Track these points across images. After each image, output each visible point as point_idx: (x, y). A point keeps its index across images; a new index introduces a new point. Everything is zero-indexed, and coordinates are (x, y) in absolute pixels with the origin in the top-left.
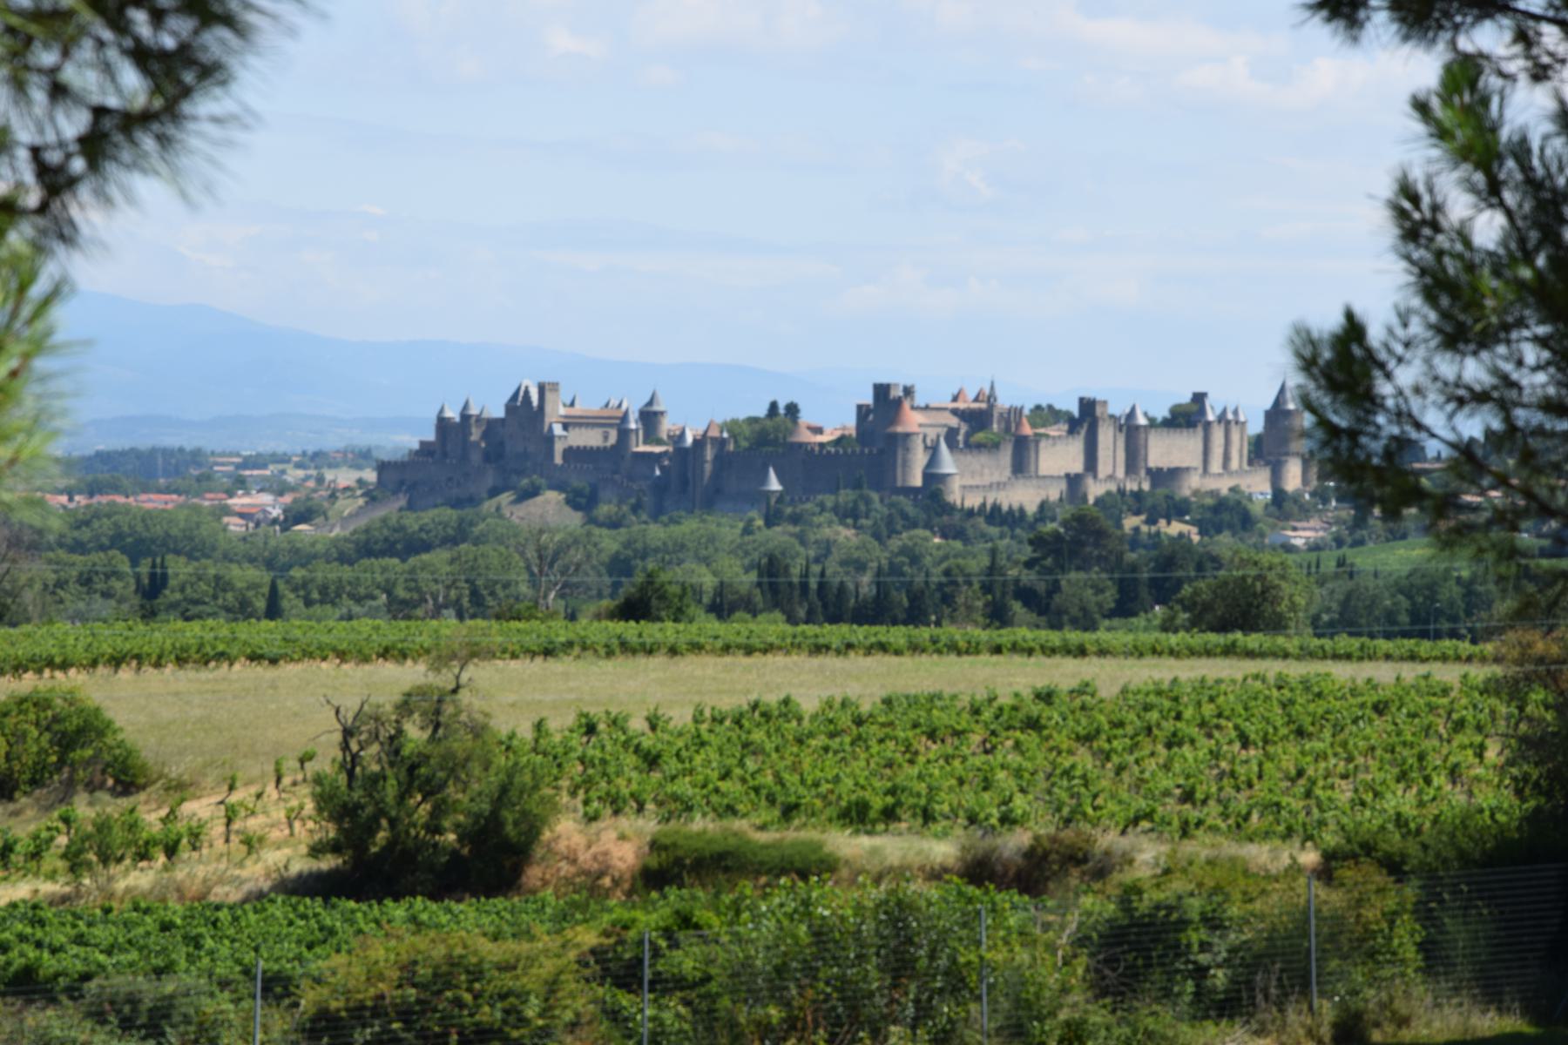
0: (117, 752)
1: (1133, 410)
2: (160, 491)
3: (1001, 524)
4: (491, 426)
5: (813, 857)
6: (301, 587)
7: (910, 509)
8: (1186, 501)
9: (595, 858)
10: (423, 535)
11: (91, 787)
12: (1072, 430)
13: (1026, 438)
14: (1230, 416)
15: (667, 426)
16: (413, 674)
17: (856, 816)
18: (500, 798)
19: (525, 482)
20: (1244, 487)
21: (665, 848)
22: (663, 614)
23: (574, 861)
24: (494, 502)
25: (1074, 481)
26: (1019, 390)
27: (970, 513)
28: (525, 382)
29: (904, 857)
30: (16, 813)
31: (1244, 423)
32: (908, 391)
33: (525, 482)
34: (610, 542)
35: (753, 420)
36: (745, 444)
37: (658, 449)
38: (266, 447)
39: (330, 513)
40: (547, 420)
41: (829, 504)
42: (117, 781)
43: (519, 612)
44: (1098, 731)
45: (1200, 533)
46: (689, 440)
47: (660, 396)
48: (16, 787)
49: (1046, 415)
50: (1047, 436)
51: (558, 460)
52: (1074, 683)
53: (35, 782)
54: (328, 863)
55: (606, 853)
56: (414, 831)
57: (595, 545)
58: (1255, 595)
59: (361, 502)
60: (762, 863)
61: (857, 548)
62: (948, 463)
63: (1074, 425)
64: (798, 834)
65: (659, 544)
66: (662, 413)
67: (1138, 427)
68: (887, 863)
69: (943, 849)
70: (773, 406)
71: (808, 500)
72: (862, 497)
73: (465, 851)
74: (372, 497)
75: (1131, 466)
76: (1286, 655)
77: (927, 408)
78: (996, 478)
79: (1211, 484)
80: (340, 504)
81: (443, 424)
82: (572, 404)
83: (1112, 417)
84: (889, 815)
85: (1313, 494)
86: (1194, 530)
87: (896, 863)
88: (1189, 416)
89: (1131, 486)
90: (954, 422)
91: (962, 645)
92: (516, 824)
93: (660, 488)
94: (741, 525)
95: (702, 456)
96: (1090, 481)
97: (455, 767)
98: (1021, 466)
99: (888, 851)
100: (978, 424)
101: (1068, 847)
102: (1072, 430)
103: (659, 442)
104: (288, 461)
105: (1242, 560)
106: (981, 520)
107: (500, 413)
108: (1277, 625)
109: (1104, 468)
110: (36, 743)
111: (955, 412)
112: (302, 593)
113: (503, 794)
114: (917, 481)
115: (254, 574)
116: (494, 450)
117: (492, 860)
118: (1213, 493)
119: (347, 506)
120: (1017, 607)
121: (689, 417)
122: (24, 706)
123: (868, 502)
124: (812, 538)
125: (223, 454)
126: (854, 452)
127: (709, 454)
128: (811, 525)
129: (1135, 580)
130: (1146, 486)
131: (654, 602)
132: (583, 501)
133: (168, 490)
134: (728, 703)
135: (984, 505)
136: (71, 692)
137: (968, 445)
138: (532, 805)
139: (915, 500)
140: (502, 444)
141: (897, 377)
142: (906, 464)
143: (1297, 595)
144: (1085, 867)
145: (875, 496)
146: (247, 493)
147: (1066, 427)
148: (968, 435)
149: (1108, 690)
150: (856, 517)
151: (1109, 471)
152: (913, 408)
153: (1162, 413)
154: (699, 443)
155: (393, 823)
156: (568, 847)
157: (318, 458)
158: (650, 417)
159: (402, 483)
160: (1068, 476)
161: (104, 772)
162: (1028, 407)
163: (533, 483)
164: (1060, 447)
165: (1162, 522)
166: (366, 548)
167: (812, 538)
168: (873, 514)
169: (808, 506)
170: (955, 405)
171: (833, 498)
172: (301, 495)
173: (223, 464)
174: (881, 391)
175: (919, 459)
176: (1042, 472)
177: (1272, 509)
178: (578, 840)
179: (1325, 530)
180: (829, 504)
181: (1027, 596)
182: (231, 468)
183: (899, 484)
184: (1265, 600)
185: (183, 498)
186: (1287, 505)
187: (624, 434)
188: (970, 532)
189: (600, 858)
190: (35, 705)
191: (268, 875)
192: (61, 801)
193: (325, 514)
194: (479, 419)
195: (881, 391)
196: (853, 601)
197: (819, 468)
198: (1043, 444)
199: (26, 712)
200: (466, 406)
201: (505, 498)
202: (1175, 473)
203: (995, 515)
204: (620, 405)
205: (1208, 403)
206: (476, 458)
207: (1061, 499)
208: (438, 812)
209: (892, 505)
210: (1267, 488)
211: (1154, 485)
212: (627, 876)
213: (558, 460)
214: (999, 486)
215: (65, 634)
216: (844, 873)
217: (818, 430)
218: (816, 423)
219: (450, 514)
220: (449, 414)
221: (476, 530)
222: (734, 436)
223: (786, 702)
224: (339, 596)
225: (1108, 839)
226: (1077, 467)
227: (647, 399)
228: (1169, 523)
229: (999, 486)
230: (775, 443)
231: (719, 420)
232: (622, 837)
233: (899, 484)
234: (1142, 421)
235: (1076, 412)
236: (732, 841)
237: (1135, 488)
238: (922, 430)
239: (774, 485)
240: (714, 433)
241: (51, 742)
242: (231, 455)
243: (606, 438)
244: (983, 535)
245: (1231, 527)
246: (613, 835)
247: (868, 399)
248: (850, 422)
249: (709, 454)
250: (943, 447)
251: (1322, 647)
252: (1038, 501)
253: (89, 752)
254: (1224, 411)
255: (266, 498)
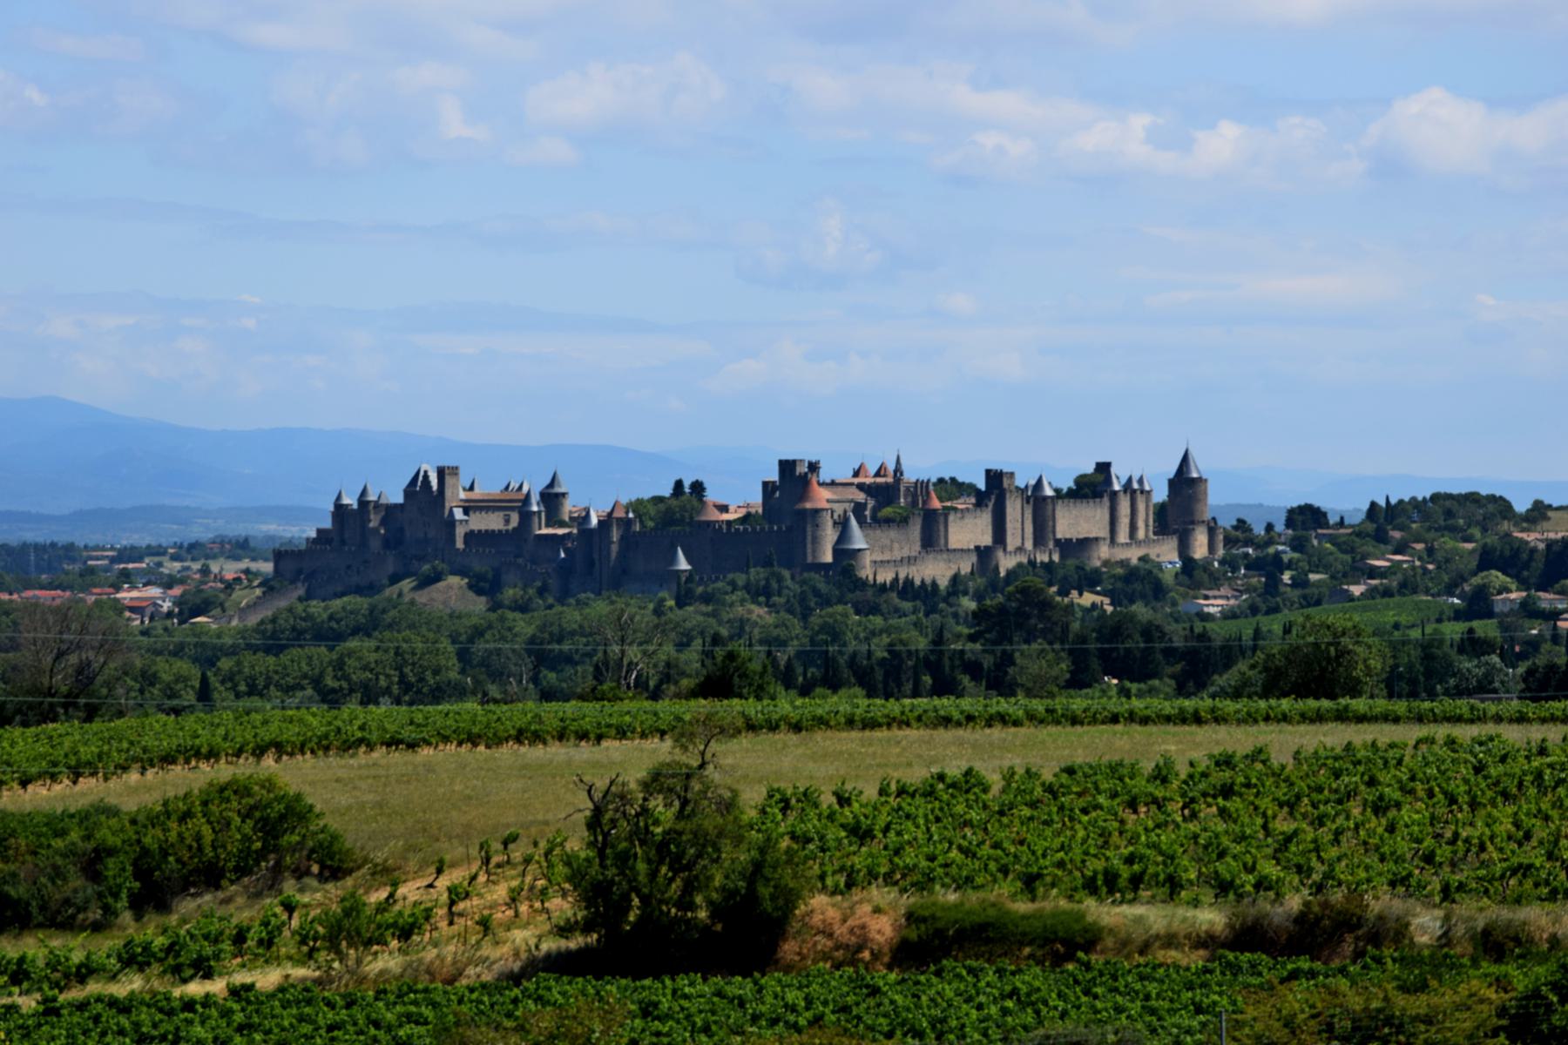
0: (321, 836)
1: (1040, 481)
2: (42, 587)
3: (914, 599)
4: (390, 512)
5: (1077, 927)
6: (229, 679)
7: (823, 587)
8: (1096, 571)
9: (851, 931)
10: (334, 625)
11: (300, 873)
12: (980, 504)
13: (935, 511)
14: (1136, 486)
15: (569, 507)
16: (662, 750)
17: (1107, 885)
18: (754, 873)
19: (426, 567)
20: (1153, 557)
21: (924, 920)
22: (745, 691)
23: (830, 935)
24: (395, 589)
25: (984, 554)
26: (921, 467)
27: (883, 588)
28: (424, 467)
29: (1170, 924)
30: (227, 901)
31: (1149, 492)
32: (814, 467)
33: (426, 567)
34: (524, 626)
35: (658, 500)
36: (651, 524)
37: (561, 531)
38: (142, 540)
39: (227, 605)
40: (447, 505)
41: (740, 583)
42: (323, 867)
43: (603, 693)
44: (1298, 797)
45: (1112, 604)
46: (594, 521)
47: (561, 477)
48: (222, 876)
49: (952, 487)
50: (955, 509)
51: (460, 544)
52: (1248, 750)
53: (242, 871)
54: (575, 943)
55: (863, 927)
56: (667, 907)
57: (510, 629)
58: (1329, 659)
59: (258, 592)
60: (1024, 934)
61: (776, 627)
62: (859, 540)
63: (981, 499)
64: (1054, 902)
65: (575, 626)
66: (564, 495)
67: (1045, 498)
68: (1153, 932)
69: (1211, 917)
70: (679, 485)
71: (717, 579)
72: (773, 574)
73: (719, 927)
74: (269, 587)
75: (1039, 540)
76: (1397, 720)
77: (833, 483)
78: (906, 553)
79: (1121, 554)
80: (237, 594)
81: (340, 510)
82: (471, 488)
83: (1018, 488)
84: (1136, 881)
85: (1222, 562)
86: (1107, 600)
87: (1162, 932)
88: (1094, 486)
89: (1042, 557)
90: (861, 497)
91: (956, 715)
92: (773, 898)
93: (566, 569)
94: (651, 606)
95: (609, 537)
96: (1000, 554)
97: (707, 844)
98: (931, 540)
99: (1152, 919)
100: (886, 499)
101: (1339, 913)
102: (980, 504)
103: (562, 524)
104: (164, 553)
105: (1314, 625)
106: (894, 595)
107: (399, 498)
108: (1354, 690)
109: (1012, 541)
110: (241, 830)
111: (861, 487)
112: (229, 685)
113: (757, 870)
114: (828, 557)
115: (183, 666)
116: (396, 534)
117: (749, 933)
118: (1124, 563)
119: (243, 597)
120: (966, 680)
121: (594, 498)
122: (226, 793)
123: (780, 579)
124: (725, 617)
125: (97, 548)
126: (762, 529)
127: (615, 535)
128: (724, 604)
129: (1086, 650)
130: (1056, 558)
131: (736, 680)
132: (487, 585)
133: (50, 586)
134: (916, 776)
135: (896, 579)
136: (269, 780)
137: (874, 518)
138: (787, 876)
139: (826, 576)
140: (402, 530)
141: (801, 452)
142: (816, 540)
143: (1371, 659)
144: (1360, 932)
145: (786, 574)
146: (133, 587)
147: (973, 500)
148: (875, 510)
149: (1280, 756)
150: (768, 595)
151: (1019, 544)
152: (820, 484)
153: (1067, 483)
154: (605, 523)
155: (645, 900)
156: (824, 921)
157: (193, 549)
158: (552, 498)
159: (300, 572)
160: (977, 548)
161: (309, 858)
162: (934, 480)
163: (434, 568)
164: (969, 521)
165: (1074, 593)
166: (272, 640)
167: (725, 617)
168: (786, 592)
169: (720, 584)
170: (856, 481)
171: (744, 576)
172: (191, 586)
173: (97, 558)
174: (787, 467)
175: (829, 536)
176: (953, 544)
177: (1183, 578)
178: (832, 913)
179: (1236, 598)
180: (740, 583)
181: (974, 670)
182: (106, 562)
183: (809, 560)
184: (1340, 665)
185: (68, 593)
186: (1198, 574)
187: (526, 516)
188: (884, 607)
189: (858, 932)
190: (235, 792)
191: (517, 954)
192: (271, 888)
193: (222, 605)
194: (377, 505)
195: (787, 467)
196: (801, 679)
197: (728, 546)
198: (951, 517)
199: (228, 800)
200: (364, 492)
201: (407, 584)
202: (1085, 544)
203: (907, 589)
204: (520, 487)
205: (1113, 470)
206: (375, 544)
207: (972, 573)
208: (689, 888)
209: (803, 582)
210: (1175, 557)
211: (1062, 557)
212: (886, 950)
213: (460, 544)
214: (910, 560)
215: (272, 717)
216: (1109, 942)
217: (724, 508)
218: (722, 501)
219: (360, 603)
220: (346, 501)
221: (388, 617)
222: (639, 516)
223: (969, 773)
224: (267, 687)
225: (1381, 902)
226: (986, 540)
227: (548, 481)
228: (1081, 594)
229: (910, 560)
230: (681, 521)
231: (624, 500)
232: (877, 910)
233: (809, 560)
234: (1049, 492)
235: (981, 485)
236: (992, 912)
237: (1046, 559)
238: (827, 506)
239: (683, 564)
240: (619, 514)
241: (254, 829)
242: (104, 549)
243: (507, 521)
244: (897, 610)
245: (1143, 596)
246: (867, 908)
247: (774, 476)
248: (756, 499)
249: (615, 535)
250: (853, 522)
251: (1432, 710)
252: (950, 573)
253: (295, 838)
254: (1130, 480)
255: (154, 591)
